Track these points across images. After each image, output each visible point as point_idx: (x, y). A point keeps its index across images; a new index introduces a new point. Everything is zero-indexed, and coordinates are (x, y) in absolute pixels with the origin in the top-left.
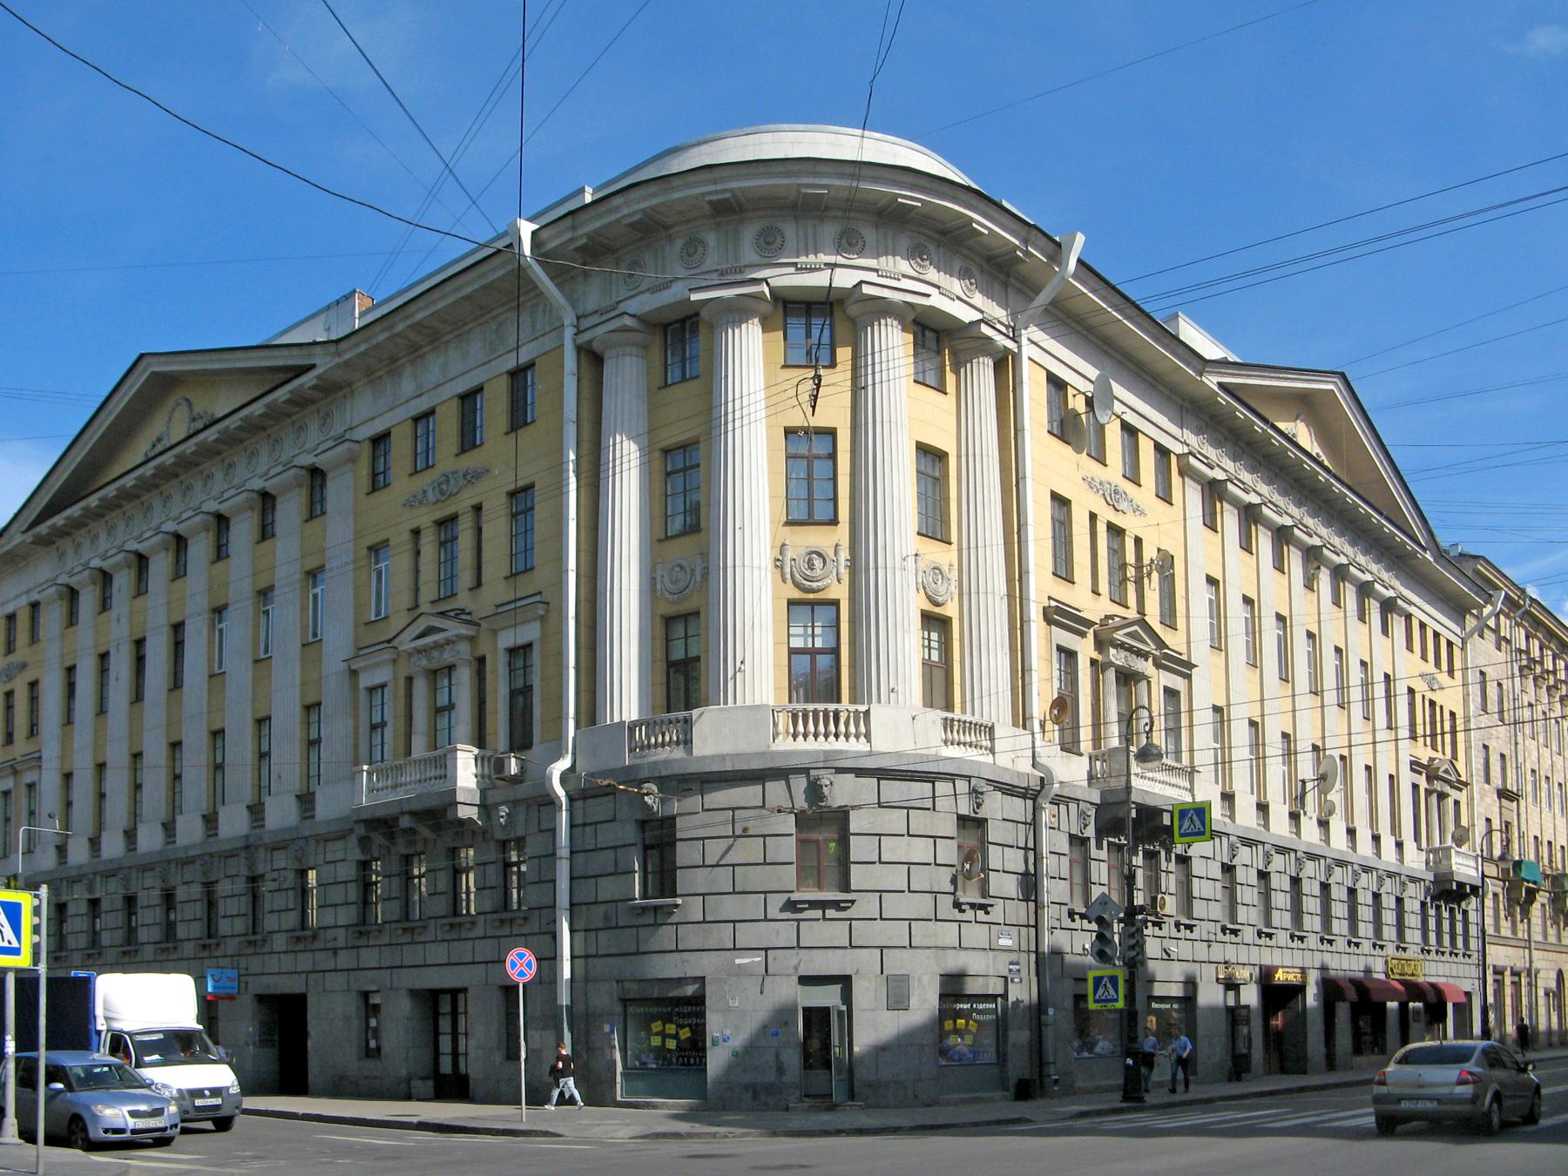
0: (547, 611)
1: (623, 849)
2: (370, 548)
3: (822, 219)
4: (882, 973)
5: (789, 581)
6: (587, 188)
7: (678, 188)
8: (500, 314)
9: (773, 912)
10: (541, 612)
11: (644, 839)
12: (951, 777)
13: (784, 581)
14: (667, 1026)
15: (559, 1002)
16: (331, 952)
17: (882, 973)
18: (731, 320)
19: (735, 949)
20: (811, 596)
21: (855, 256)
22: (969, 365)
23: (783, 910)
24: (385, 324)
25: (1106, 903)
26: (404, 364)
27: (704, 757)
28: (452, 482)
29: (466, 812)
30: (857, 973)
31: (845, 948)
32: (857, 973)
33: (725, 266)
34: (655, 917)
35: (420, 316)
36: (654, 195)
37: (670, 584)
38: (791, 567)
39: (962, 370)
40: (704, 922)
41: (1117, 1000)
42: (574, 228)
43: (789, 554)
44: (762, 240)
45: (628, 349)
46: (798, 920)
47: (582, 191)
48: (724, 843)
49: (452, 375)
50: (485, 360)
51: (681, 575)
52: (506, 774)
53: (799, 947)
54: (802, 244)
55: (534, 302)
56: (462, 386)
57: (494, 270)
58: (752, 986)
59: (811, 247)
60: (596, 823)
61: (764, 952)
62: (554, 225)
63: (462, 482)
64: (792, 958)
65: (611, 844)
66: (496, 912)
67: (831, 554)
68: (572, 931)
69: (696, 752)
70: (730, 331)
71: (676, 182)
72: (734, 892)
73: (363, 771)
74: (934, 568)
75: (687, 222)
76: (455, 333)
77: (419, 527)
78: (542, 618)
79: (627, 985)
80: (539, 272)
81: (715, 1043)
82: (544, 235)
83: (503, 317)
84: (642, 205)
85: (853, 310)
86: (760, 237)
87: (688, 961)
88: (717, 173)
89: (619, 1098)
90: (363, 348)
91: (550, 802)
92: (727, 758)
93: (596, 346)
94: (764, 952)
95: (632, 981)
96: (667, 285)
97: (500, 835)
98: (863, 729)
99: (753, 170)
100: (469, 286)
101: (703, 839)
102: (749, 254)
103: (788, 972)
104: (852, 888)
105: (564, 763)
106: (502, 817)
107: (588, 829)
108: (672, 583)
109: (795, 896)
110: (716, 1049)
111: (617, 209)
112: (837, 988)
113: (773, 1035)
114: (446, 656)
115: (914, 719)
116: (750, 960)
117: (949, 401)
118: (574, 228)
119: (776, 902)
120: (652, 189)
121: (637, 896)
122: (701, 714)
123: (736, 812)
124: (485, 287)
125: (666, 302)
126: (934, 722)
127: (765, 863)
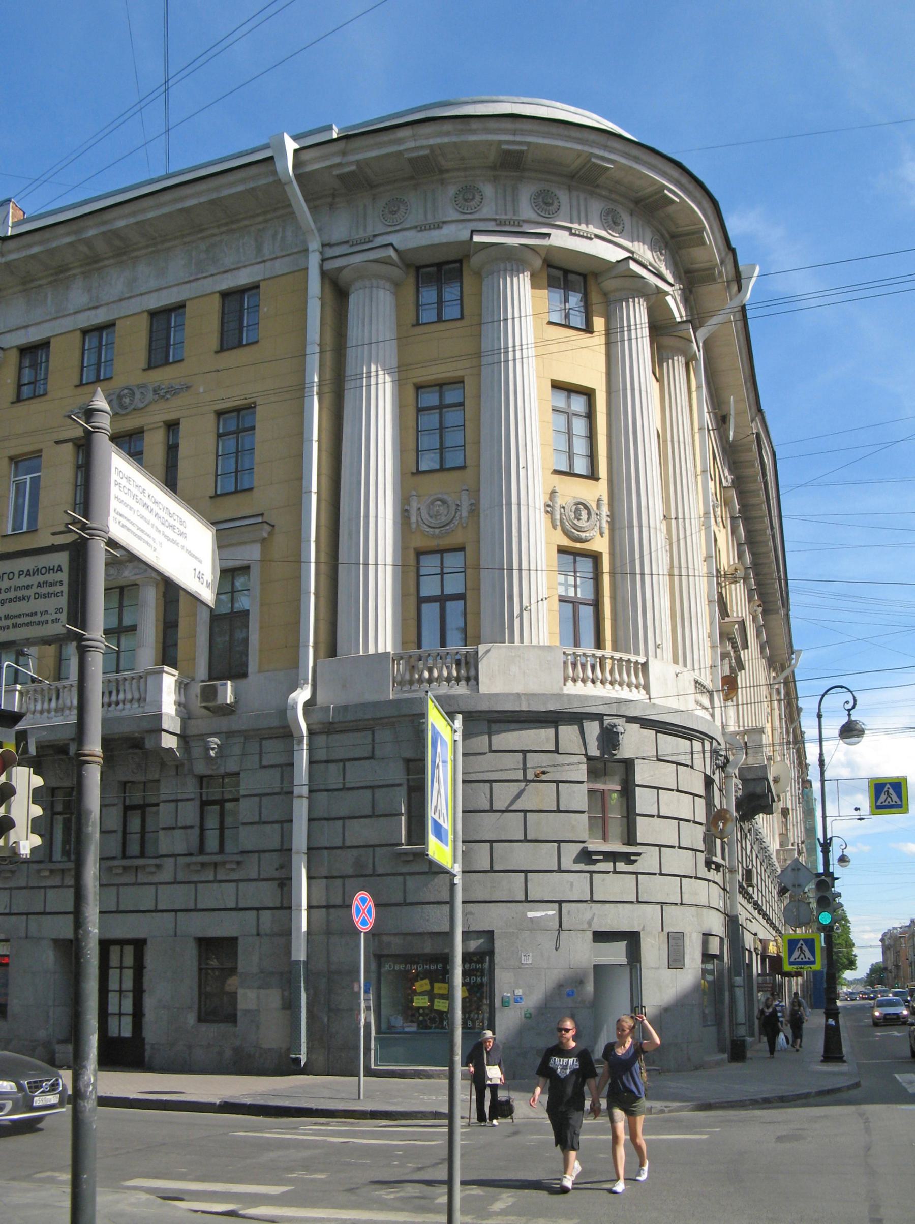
0: (271, 534)
1: (183, 803)
2: (11, 459)
3: (592, 193)
4: (662, 930)
5: (559, 528)
6: (334, 127)
7: (474, 132)
8: (214, 235)
9: (568, 862)
10: (265, 535)
11: (201, 794)
12: (577, 719)
13: (554, 527)
14: (436, 985)
15: (294, 958)
16: (276, 883)
17: (662, 930)
18: (509, 268)
19: (527, 901)
20: (578, 545)
21: (617, 235)
22: (670, 361)
23: (577, 860)
24: (74, 226)
25: (799, 869)
26: (75, 275)
27: (497, 695)
28: (138, 396)
29: (169, 742)
30: (643, 930)
31: (632, 902)
32: (643, 930)
33: (503, 217)
34: (136, 876)
35: (121, 223)
36: (448, 134)
37: (427, 516)
38: (561, 514)
39: (665, 365)
40: (492, 871)
41: (813, 963)
42: (344, 153)
43: (560, 501)
44: (541, 200)
45: (382, 282)
46: (591, 873)
47: (330, 128)
48: (515, 788)
49: (143, 290)
50: (192, 278)
51: (443, 510)
52: (220, 701)
53: (638, 902)
54: (575, 214)
55: (260, 227)
56: (155, 302)
57: (231, 185)
58: (547, 941)
59: (583, 219)
60: (343, 761)
61: (557, 905)
62: (319, 147)
63: (150, 396)
64: (586, 912)
65: (368, 784)
66: (191, 855)
67: (594, 506)
68: (309, 878)
69: (484, 689)
70: (508, 279)
71: (475, 125)
72: (526, 840)
73: (16, 690)
74: (577, 504)
75: (465, 169)
76: (150, 249)
77: (143, 427)
78: (263, 541)
79: (385, 939)
80: (296, 193)
81: (505, 1003)
82: (306, 156)
83: (217, 239)
84: (431, 142)
85: (610, 284)
86: (539, 195)
87: (471, 913)
88: (519, 125)
89: (373, 1067)
90: (36, 250)
91: (287, 734)
92: (523, 697)
93: (345, 275)
94: (557, 905)
95: (395, 935)
96: (438, 226)
97: (201, 768)
98: (642, 681)
99: (554, 129)
100: (192, 199)
101: (490, 782)
102: (526, 211)
103: (580, 927)
104: (638, 841)
105: (302, 696)
106: (213, 749)
107: (332, 767)
108: (431, 517)
109: (592, 847)
110: (506, 1010)
111: (400, 141)
112: (621, 946)
113: (568, 995)
114: (126, 573)
115: (677, 676)
116: (543, 914)
117: (598, 340)
118: (344, 153)
119: (570, 852)
120: (448, 126)
121: (403, 842)
122: (488, 651)
123: (528, 755)
124: (212, 202)
125: (437, 241)
126: (690, 681)
127: (558, 811)
